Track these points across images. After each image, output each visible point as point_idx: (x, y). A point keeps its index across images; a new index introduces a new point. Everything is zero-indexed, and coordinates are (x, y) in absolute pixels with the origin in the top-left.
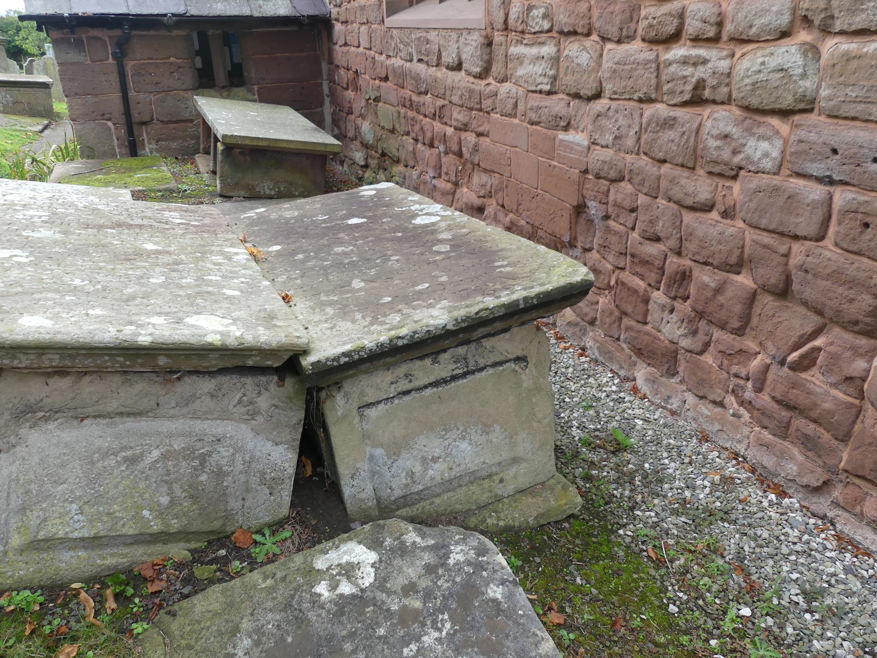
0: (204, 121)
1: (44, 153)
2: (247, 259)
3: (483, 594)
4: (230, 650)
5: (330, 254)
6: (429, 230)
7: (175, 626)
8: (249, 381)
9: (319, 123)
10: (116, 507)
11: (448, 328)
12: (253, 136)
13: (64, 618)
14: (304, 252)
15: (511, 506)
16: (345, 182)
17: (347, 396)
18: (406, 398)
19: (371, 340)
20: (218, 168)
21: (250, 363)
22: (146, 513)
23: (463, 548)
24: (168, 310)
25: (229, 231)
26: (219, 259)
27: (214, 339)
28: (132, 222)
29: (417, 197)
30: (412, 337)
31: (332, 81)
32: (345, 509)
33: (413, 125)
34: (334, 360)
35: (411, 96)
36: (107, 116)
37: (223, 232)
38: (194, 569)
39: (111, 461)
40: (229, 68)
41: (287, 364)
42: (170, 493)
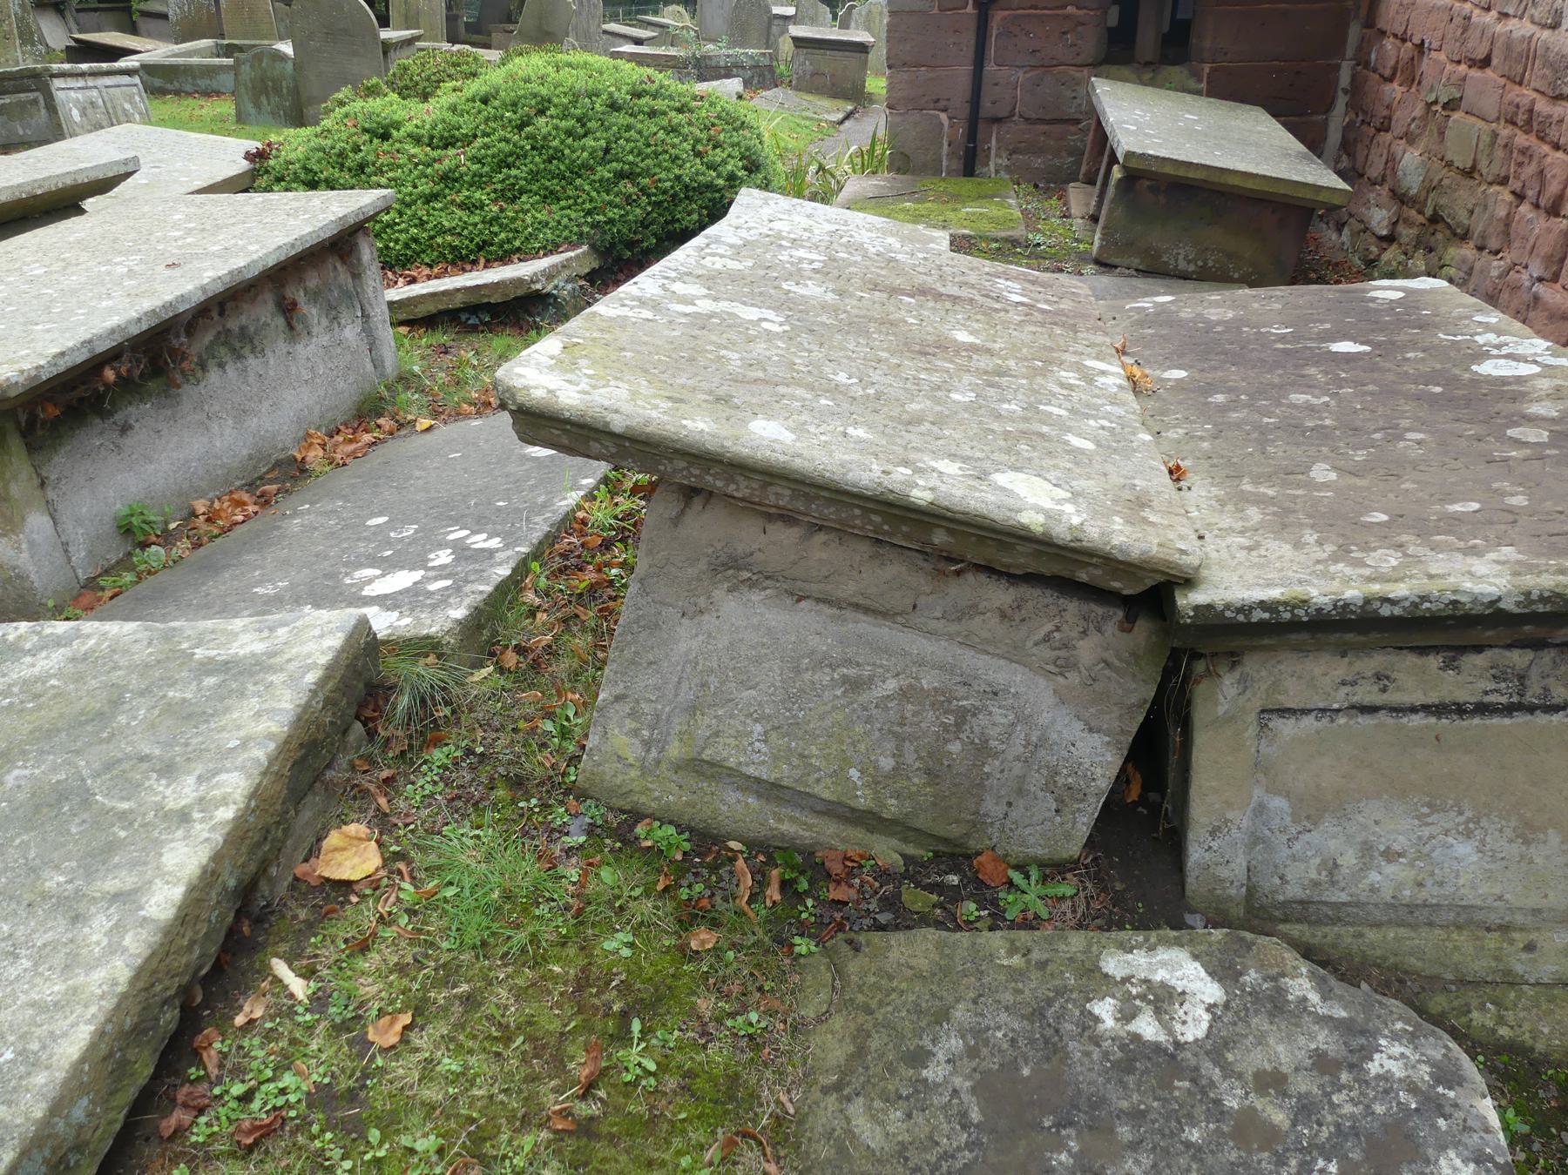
0: (1099, 123)
1: (837, 159)
2: (1120, 387)
3: (1428, 1162)
4: (926, 1042)
5: (1279, 404)
6: (1510, 392)
7: (853, 967)
8: (1073, 607)
9: (1314, 143)
10: (814, 750)
11: (1502, 605)
12: (1181, 158)
13: (710, 888)
14: (1230, 391)
15: (1538, 1006)
16: (1337, 264)
17: (1244, 683)
18: (1365, 721)
19: (1327, 589)
20: (1104, 212)
21: (1083, 576)
22: (854, 773)
23: (1408, 1052)
24: (969, 453)
25: (1100, 329)
26: (1070, 377)
27: (1032, 520)
28: (942, 290)
29: (1494, 317)
30: (1415, 605)
31: (1362, 61)
32: (1182, 884)
33: (1520, 164)
34: (1240, 610)
35: (1533, 102)
36: (942, 104)
37: (1088, 330)
38: (903, 889)
39: (824, 677)
40: (1166, 29)
41: (1145, 596)
42: (898, 755)
